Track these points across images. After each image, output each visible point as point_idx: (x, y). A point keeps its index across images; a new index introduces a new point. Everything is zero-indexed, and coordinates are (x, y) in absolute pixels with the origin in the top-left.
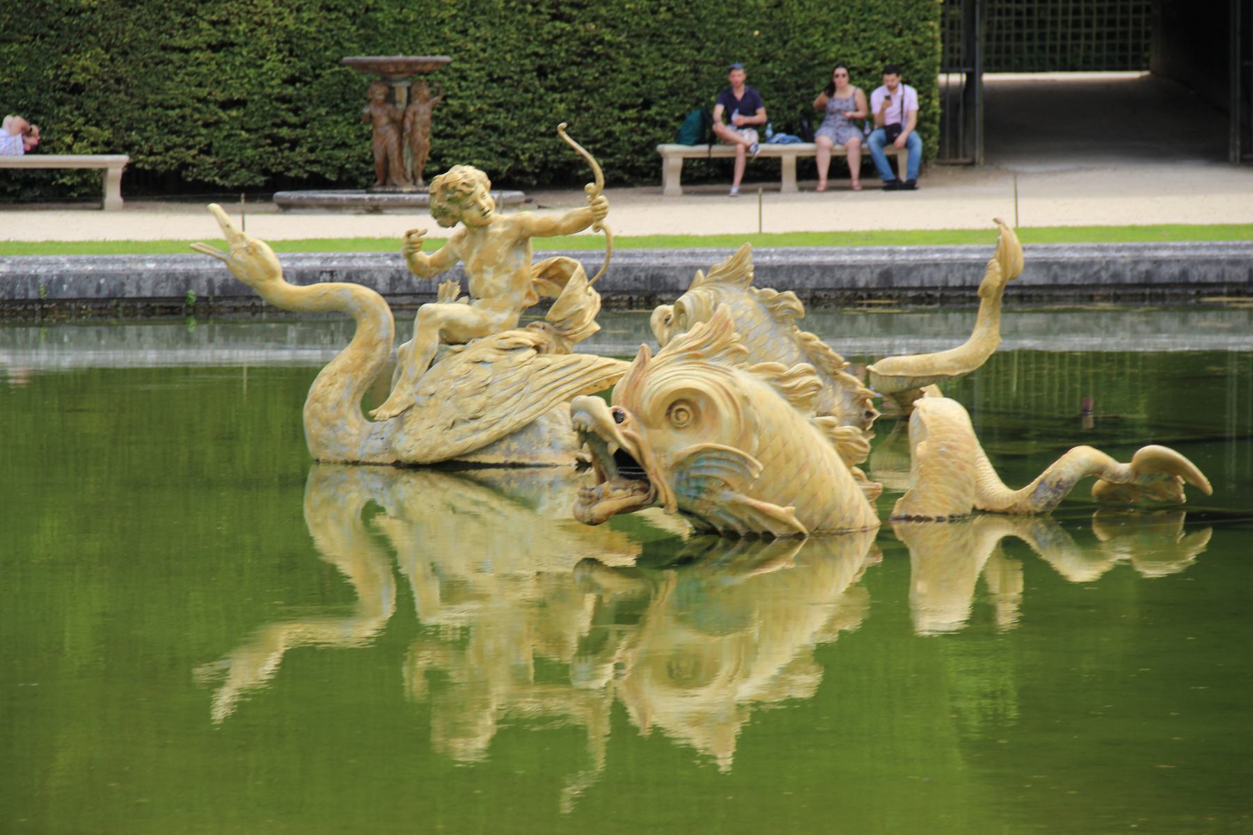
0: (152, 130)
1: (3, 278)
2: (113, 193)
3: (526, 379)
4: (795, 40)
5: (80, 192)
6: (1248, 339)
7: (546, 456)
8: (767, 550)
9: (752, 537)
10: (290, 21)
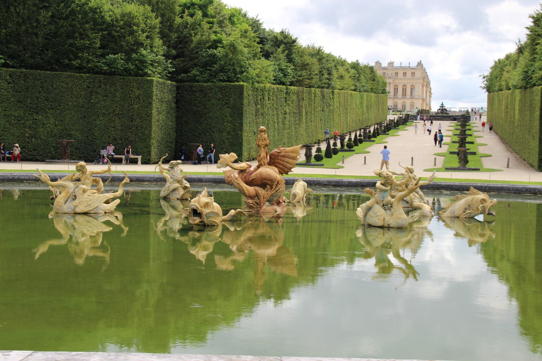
1: (2, 178)
2: (139, 162)
3: (98, 198)
6: (2, 188)
7: (100, 211)
8: (215, 228)
9: (212, 226)
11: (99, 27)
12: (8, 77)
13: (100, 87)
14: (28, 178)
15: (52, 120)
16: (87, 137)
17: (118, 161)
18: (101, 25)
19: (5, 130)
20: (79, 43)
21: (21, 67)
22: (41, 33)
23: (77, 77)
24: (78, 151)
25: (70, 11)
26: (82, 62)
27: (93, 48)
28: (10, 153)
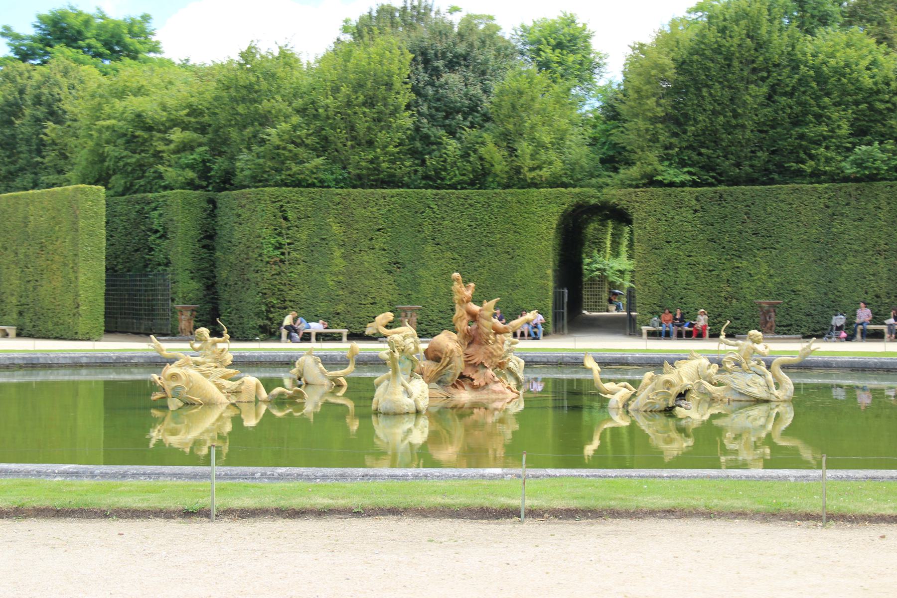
0: (356, 324)
2: (345, 339)
4: (515, 303)
5: (337, 338)
10: (390, 297)
11: (850, 99)
12: (694, 202)
13: (848, 204)
14: (545, 360)
15: (764, 268)
16: (826, 294)
17: (877, 336)
18: (856, 94)
19: (689, 287)
20: (812, 130)
21: (720, 182)
22: (749, 124)
23: (807, 191)
24: (809, 319)
25: (800, 80)
26: (817, 165)
27: (838, 137)
28: (691, 325)
